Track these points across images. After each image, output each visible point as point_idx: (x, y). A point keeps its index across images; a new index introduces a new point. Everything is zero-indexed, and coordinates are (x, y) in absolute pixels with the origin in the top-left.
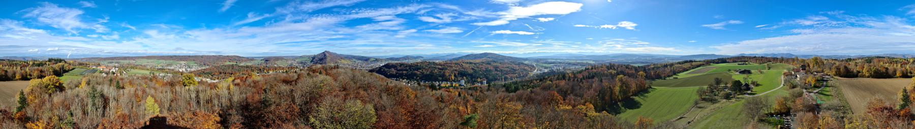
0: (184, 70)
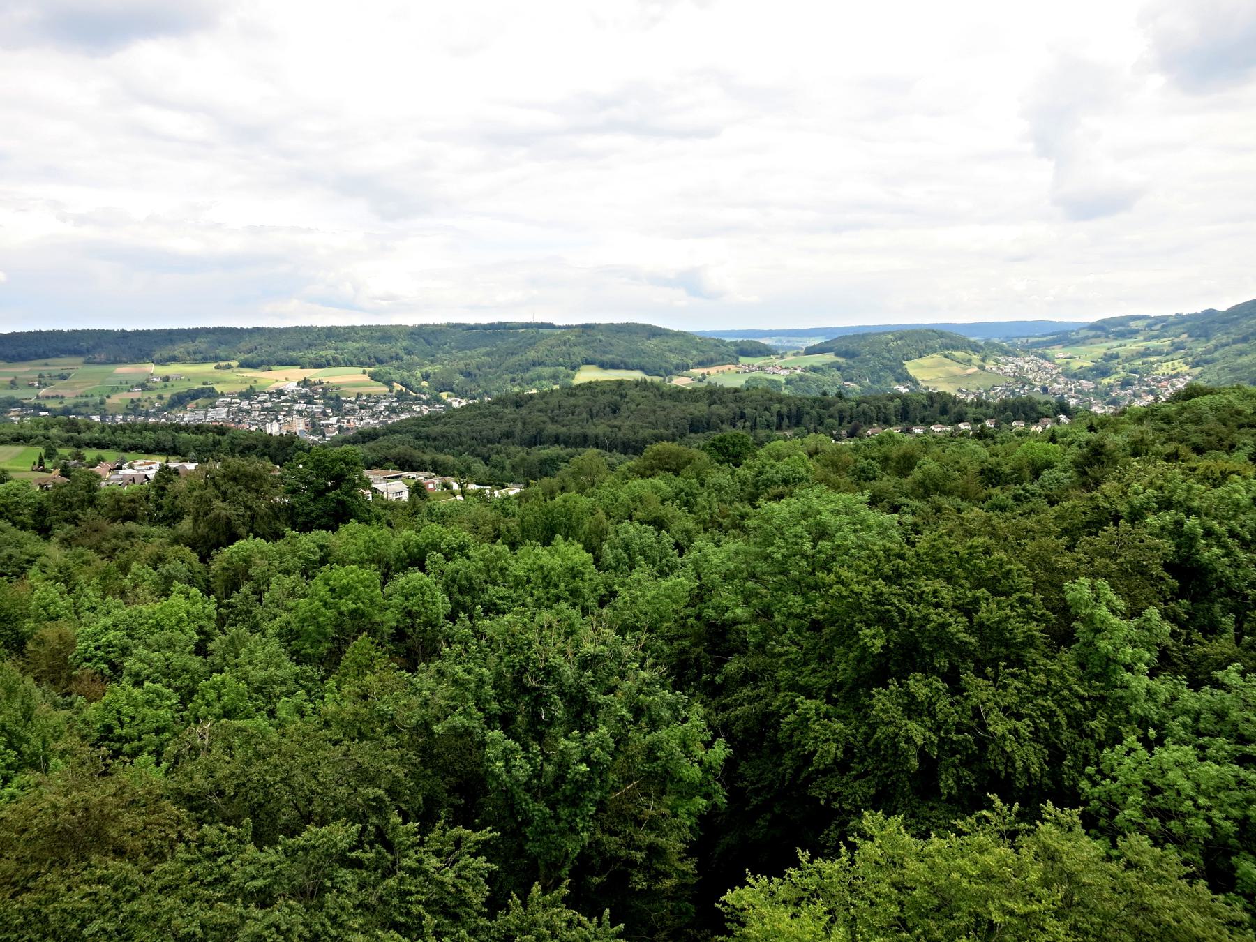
0: (299, 426)
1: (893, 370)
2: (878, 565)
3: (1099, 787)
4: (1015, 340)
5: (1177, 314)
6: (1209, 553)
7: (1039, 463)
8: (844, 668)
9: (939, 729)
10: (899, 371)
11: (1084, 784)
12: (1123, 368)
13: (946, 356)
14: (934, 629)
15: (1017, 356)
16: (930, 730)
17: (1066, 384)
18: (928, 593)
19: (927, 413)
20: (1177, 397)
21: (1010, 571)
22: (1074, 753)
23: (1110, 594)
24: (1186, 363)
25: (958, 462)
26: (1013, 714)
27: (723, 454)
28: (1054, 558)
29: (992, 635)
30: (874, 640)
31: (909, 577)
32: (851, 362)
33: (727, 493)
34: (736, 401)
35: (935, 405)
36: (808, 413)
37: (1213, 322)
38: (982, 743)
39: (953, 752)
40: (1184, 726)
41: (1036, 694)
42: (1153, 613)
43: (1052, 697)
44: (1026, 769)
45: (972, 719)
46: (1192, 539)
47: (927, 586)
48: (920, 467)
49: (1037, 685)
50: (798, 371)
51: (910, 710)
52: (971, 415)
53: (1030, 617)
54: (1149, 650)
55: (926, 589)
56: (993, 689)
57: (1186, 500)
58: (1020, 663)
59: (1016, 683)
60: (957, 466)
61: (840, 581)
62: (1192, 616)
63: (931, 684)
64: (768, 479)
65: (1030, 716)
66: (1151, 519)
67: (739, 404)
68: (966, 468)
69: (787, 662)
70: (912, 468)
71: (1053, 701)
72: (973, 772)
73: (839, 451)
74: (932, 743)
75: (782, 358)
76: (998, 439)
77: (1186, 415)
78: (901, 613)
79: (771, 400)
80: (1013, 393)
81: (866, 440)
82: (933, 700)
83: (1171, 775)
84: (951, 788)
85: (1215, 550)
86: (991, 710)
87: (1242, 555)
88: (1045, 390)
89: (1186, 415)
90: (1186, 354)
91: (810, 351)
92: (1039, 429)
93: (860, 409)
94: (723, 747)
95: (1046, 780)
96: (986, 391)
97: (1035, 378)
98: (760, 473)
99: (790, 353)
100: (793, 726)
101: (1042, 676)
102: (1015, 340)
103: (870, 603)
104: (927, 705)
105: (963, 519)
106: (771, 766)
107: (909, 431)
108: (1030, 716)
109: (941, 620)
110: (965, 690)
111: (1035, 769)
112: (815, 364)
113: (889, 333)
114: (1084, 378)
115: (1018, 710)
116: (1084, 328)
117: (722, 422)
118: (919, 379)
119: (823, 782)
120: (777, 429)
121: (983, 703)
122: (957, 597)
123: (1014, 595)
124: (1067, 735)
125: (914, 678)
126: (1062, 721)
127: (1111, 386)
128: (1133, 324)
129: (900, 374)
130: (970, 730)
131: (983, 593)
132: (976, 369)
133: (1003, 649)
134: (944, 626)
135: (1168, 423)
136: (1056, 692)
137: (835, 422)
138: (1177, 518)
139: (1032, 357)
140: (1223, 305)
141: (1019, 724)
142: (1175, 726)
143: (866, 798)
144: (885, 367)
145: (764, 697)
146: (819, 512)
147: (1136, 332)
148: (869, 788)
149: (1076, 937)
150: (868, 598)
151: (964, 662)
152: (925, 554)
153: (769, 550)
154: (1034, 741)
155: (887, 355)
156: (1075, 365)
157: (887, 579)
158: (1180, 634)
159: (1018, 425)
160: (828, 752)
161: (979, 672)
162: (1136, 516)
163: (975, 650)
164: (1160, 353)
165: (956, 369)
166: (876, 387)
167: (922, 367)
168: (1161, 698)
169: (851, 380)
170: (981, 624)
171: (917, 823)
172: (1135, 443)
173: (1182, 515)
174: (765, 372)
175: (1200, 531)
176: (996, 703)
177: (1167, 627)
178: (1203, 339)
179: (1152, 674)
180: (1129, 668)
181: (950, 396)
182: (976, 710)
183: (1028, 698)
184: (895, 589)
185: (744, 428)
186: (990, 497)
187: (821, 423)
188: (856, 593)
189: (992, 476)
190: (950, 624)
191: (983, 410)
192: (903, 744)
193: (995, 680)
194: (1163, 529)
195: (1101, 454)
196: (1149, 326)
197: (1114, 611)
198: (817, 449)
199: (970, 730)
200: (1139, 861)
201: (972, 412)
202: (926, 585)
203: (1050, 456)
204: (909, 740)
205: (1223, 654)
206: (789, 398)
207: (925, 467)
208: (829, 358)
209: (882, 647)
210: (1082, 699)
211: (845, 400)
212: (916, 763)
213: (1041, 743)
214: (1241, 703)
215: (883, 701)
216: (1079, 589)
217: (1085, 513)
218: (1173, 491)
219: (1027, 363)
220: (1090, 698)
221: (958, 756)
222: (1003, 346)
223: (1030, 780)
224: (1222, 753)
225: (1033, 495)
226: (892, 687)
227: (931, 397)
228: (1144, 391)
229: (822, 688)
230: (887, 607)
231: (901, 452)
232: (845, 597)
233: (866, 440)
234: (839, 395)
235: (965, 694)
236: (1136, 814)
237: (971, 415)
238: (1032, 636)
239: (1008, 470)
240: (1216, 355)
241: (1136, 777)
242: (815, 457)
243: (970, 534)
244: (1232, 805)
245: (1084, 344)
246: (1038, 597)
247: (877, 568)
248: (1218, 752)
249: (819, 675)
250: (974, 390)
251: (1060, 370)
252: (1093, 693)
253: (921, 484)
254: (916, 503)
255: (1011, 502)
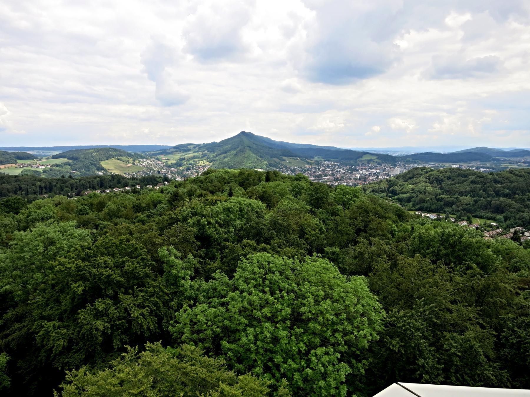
1: (95, 165)
2: (78, 254)
3: (176, 328)
4: (146, 153)
5: (204, 144)
6: (210, 231)
7: (156, 202)
8: (66, 302)
9: (111, 321)
10: (98, 165)
11: (170, 328)
12: (187, 163)
13: (118, 159)
14: (106, 278)
15: (147, 159)
16: (107, 322)
17: (167, 170)
18: (101, 263)
19: (111, 184)
20: (205, 174)
21: (137, 248)
22: (167, 317)
23: (175, 251)
24: (208, 161)
25: (123, 204)
26: (142, 307)
27: (9, 208)
28: (155, 240)
29: (131, 276)
30: (78, 288)
31: (93, 257)
32: (75, 162)
33: (10, 228)
34: (16, 181)
35: (115, 180)
36: (55, 186)
37: (215, 146)
38: (129, 322)
39: (118, 329)
40: (204, 296)
41: (150, 296)
42: (191, 256)
43: (156, 296)
44: (148, 328)
45: (124, 313)
46: (204, 226)
47: (101, 260)
48: (107, 207)
49: (150, 293)
50: (49, 167)
51: (97, 316)
52: (130, 184)
53: (145, 265)
54: (191, 270)
55: (100, 261)
56: (132, 298)
57: (201, 212)
58: (143, 285)
59: (142, 294)
60: (123, 205)
61: (60, 264)
62: (206, 255)
63: (106, 302)
64: (33, 218)
65: (148, 306)
66: (190, 221)
67: (18, 183)
68: (127, 206)
69: (38, 306)
70: (104, 208)
71: (157, 298)
72: (127, 335)
73: (69, 203)
74: (108, 328)
75: (40, 160)
76: (142, 193)
77: (207, 180)
78: (90, 273)
79: (35, 180)
80: (147, 174)
81: (84, 197)
82: (107, 309)
83: (198, 317)
84: (118, 345)
85: (212, 229)
86: (132, 307)
87: (221, 230)
88: (159, 172)
89: (207, 180)
90: (208, 158)
91: (54, 157)
92: (158, 188)
93: (81, 183)
94: (5, 357)
95: (157, 330)
96: (136, 173)
97: (155, 168)
98: (29, 216)
99: (44, 158)
100: (42, 337)
101: (152, 289)
102: (146, 153)
103: (76, 271)
104: (104, 312)
105: (117, 228)
106: (35, 358)
107: (104, 191)
108: (148, 306)
109: (108, 274)
110: (120, 301)
111: (152, 327)
112: (58, 163)
113: (92, 149)
114: (173, 167)
115: (143, 305)
116: (171, 148)
117: (9, 192)
118: (107, 169)
119: (59, 359)
120: (40, 194)
121: (128, 305)
122: (116, 262)
123: (139, 258)
124: (163, 310)
125: (98, 301)
126: (161, 305)
127: (183, 170)
128: (189, 147)
129: (99, 167)
130: (124, 318)
131: (126, 259)
132: (131, 165)
133: (136, 281)
134: (109, 276)
135: (202, 183)
136: (158, 294)
137: (69, 189)
138: (198, 219)
139: (153, 159)
140: (218, 141)
141: (144, 310)
142: (201, 297)
143: (80, 360)
144: (92, 164)
145: (27, 326)
146: (48, 233)
147: (190, 150)
148: (82, 356)
149: (160, 394)
150: (74, 269)
151: (120, 290)
152: (100, 245)
153: (22, 255)
154: (151, 316)
155: (92, 159)
156: (170, 163)
157: (84, 260)
158: (202, 262)
159: (149, 187)
160: (60, 345)
161: (126, 293)
162: (185, 219)
163: (124, 283)
164: (199, 158)
165: (122, 164)
166: (88, 173)
167: (108, 164)
168: (195, 287)
169: (76, 170)
170: (126, 272)
171: (105, 364)
172: (189, 191)
173: (200, 218)
174: (32, 167)
175: (206, 223)
176: (135, 304)
177: (197, 260)
178: (212, 152)
179: (192, 279)
180: (183, 279)
181: (121, 176)
182: (126, 309)
183: (147, 299)
184: (87, 263)
185: (21, 194)
186: (137, 217)
187: (62, 190)
188: (68, 268)
189: (138, 208)
190: (112, 275)
191: (135, 181)
192: (94, 332)
193: (133, 294)
194: (194, 223)
195: (177, 196)
196: (194, 148)
197: (176, 257)
198: (60, 202)
199: (124, 318)
200: (186, 354)
201: (130, 182)
202: (101, 259)
203: (160, 199)
204: (97, 329)
205: (216, 267)
206: (45, 179)
207: (109, 207)
208: (65, 160)
209: (83, 291)
210: (168, 295)
211: (73, 179)
212: (101, 339)
213: (153, 316)
214: (221, 283)
215: (83, 315)
216: (163, 251)
217: (167, 220)
218: (197, 209)
219: (151, 162)
220: (171, 293)
221: (120, 330)
222: (141, 155)
223: (150, 332)
224: (216, 303)
225: (154, 214)
226: (88, 308)
227: (113, 176)
228: (194, 172)
229: (56, 315)
230: (83, 272)
231: (98, 201)
232: (63, 271)
233: (84, 197)
234: (70, 177)
235: (121, 303)
236: (188, 335)
237: (130, 184)
238: (147, 273)
239: (144, 205)
240: (217, 158)
241: (187, 321)
242: (59, 206)
243: (120, 234)
244: (219, 322)
245: (172, 154)
246: (149, 257)
247: (78, 256)
248: (214, 303)
249: (54, 309)
250: (131, 173)
251: (164, 164)
252: (171, 291)
253: (108, 214)
254: (106, 223)
255: (146, 218)
